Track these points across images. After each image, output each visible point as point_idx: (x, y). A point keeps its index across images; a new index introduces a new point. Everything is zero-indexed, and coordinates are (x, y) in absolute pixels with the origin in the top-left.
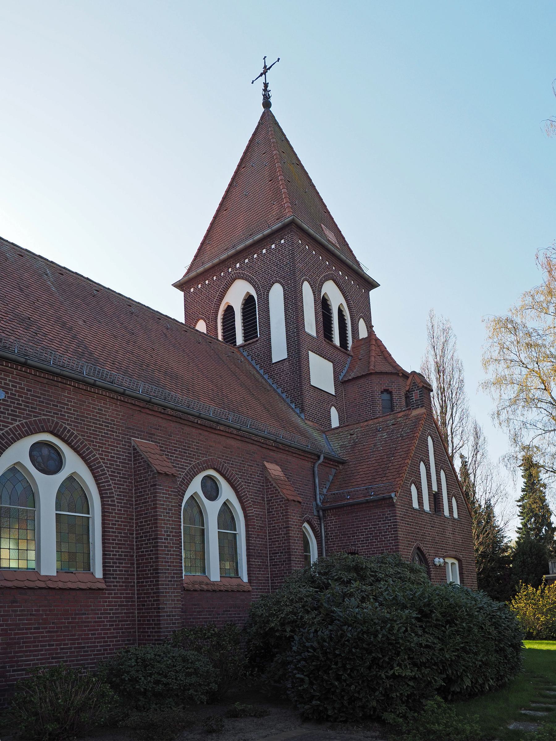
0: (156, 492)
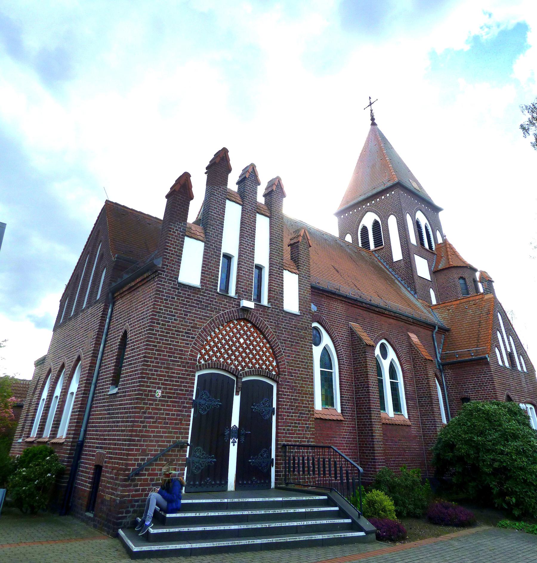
0: (366, 357)
